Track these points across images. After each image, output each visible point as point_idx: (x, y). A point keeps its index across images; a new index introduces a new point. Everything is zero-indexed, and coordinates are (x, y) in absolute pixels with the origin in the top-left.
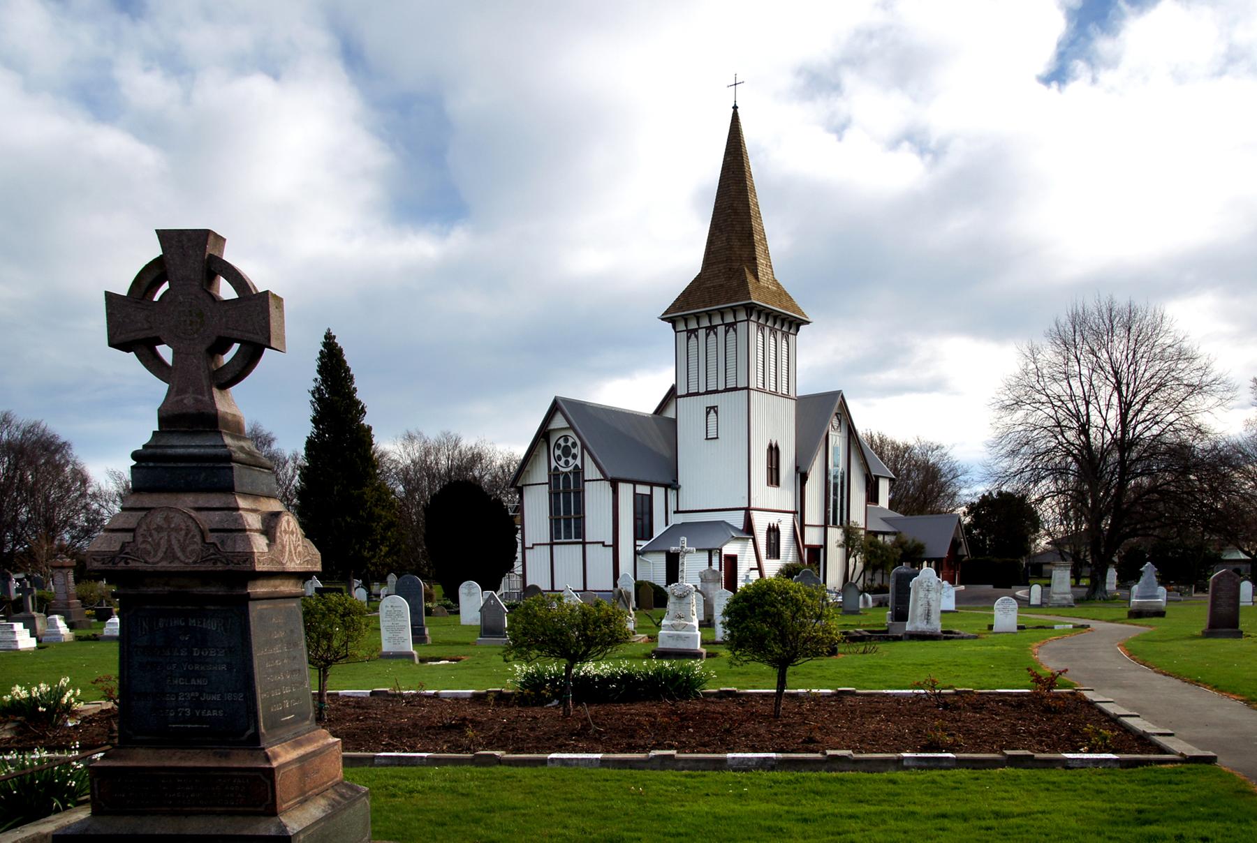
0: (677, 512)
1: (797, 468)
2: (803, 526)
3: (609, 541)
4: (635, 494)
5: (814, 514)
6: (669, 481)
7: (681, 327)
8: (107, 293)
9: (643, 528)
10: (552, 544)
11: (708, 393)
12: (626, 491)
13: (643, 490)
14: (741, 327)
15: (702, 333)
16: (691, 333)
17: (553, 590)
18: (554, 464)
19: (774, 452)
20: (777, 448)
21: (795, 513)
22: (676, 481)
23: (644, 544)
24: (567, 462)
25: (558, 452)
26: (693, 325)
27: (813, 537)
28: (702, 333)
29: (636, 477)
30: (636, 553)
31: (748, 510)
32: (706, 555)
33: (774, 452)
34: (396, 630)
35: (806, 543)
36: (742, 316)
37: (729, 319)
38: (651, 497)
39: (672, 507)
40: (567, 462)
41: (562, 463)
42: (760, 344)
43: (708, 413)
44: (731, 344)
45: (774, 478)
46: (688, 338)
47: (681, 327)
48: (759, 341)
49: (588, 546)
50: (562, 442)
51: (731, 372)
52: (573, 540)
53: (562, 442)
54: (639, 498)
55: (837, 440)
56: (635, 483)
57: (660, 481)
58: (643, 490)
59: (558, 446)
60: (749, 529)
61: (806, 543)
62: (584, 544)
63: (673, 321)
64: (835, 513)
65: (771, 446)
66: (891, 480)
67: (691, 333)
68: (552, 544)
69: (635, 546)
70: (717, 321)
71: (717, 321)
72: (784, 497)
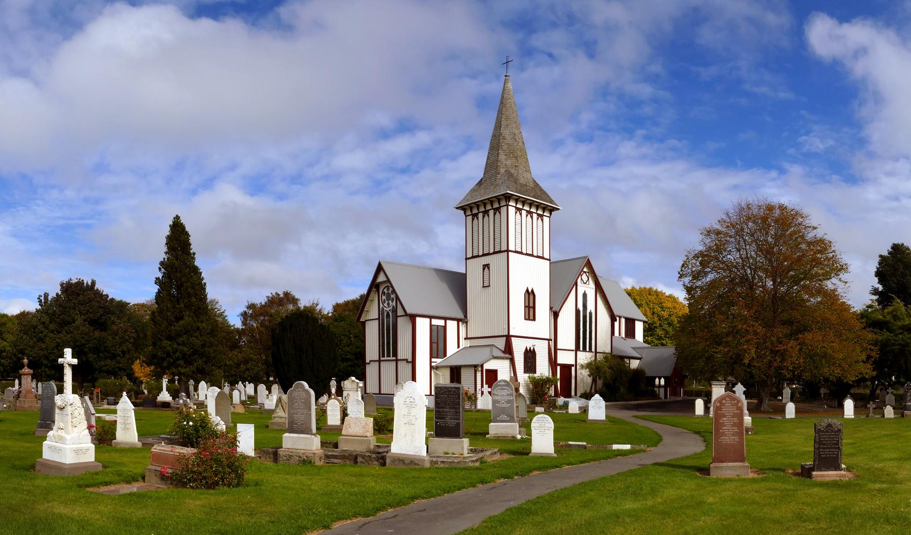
0: (466, 338)
1: (551, 308)
2: (556, 349)
3: (410, 360)
4: (431, 325)
5: (567, 338)
6: (461, 316)
7: (469, 213)
8: (177, 217)
9: (438, 346)
10: (380, 361)
11: (484, 255)
12: (423, 325)
13: (441, 323)
14: (504, 210)
15: (480, 215)
16: (475, 216)
17: (380, 393)
18: (381, 305)
19: (530, 295)
20: (532, 291)
21: (549, 340)
22: (466, 317)
23: (439, 361)
24: (388, 304)
25: (384, 298)
26: (475, 211)
27: (564, 358)
28: (480, 215)
29: (431, 314)
30: (431, 367)
31: (508, 338)
32: (472, 370)
33: (530, 295)
34: (126, 429)
35: (559, 361)
36: (503, 203)
37: (496, 205)
38: (445, 327)
39: (463, 334)
40: (388, 304)
41: (386, 305)
42: (519, 221)
43: (484, 269)
44: (497, 221)
45: (530, 312)
46: (473, 219)
47: (469, 213)
48: (518, 225)
49: (399, 363)
50: (385, 290)
51: (497, 241)
52: (386, 358)
53: (385, 290)
54: (434, 329)
55: (587, 287)
56: (431, 317)
57: (453, 316)
58: (441, 323)
59: (383, 293)
60: (508, 350)
61: (559, 361)
62: (397, 361)
63: (462, 208)
64: (583, 338)
65: (527, 291)
66: (644, 322)
67: (475, 216)
68: (380, 361)
69: (431, 362)
70: (489, 207)
71: (489, 207)
72: (542, 326)
